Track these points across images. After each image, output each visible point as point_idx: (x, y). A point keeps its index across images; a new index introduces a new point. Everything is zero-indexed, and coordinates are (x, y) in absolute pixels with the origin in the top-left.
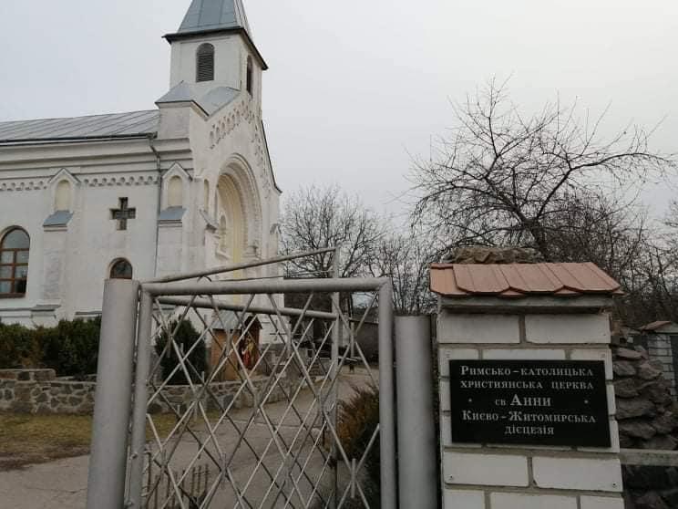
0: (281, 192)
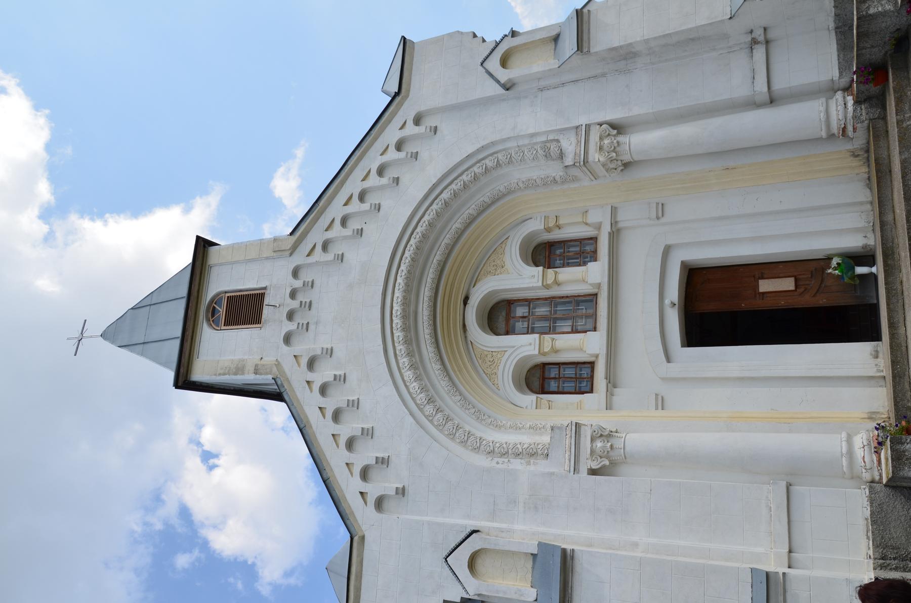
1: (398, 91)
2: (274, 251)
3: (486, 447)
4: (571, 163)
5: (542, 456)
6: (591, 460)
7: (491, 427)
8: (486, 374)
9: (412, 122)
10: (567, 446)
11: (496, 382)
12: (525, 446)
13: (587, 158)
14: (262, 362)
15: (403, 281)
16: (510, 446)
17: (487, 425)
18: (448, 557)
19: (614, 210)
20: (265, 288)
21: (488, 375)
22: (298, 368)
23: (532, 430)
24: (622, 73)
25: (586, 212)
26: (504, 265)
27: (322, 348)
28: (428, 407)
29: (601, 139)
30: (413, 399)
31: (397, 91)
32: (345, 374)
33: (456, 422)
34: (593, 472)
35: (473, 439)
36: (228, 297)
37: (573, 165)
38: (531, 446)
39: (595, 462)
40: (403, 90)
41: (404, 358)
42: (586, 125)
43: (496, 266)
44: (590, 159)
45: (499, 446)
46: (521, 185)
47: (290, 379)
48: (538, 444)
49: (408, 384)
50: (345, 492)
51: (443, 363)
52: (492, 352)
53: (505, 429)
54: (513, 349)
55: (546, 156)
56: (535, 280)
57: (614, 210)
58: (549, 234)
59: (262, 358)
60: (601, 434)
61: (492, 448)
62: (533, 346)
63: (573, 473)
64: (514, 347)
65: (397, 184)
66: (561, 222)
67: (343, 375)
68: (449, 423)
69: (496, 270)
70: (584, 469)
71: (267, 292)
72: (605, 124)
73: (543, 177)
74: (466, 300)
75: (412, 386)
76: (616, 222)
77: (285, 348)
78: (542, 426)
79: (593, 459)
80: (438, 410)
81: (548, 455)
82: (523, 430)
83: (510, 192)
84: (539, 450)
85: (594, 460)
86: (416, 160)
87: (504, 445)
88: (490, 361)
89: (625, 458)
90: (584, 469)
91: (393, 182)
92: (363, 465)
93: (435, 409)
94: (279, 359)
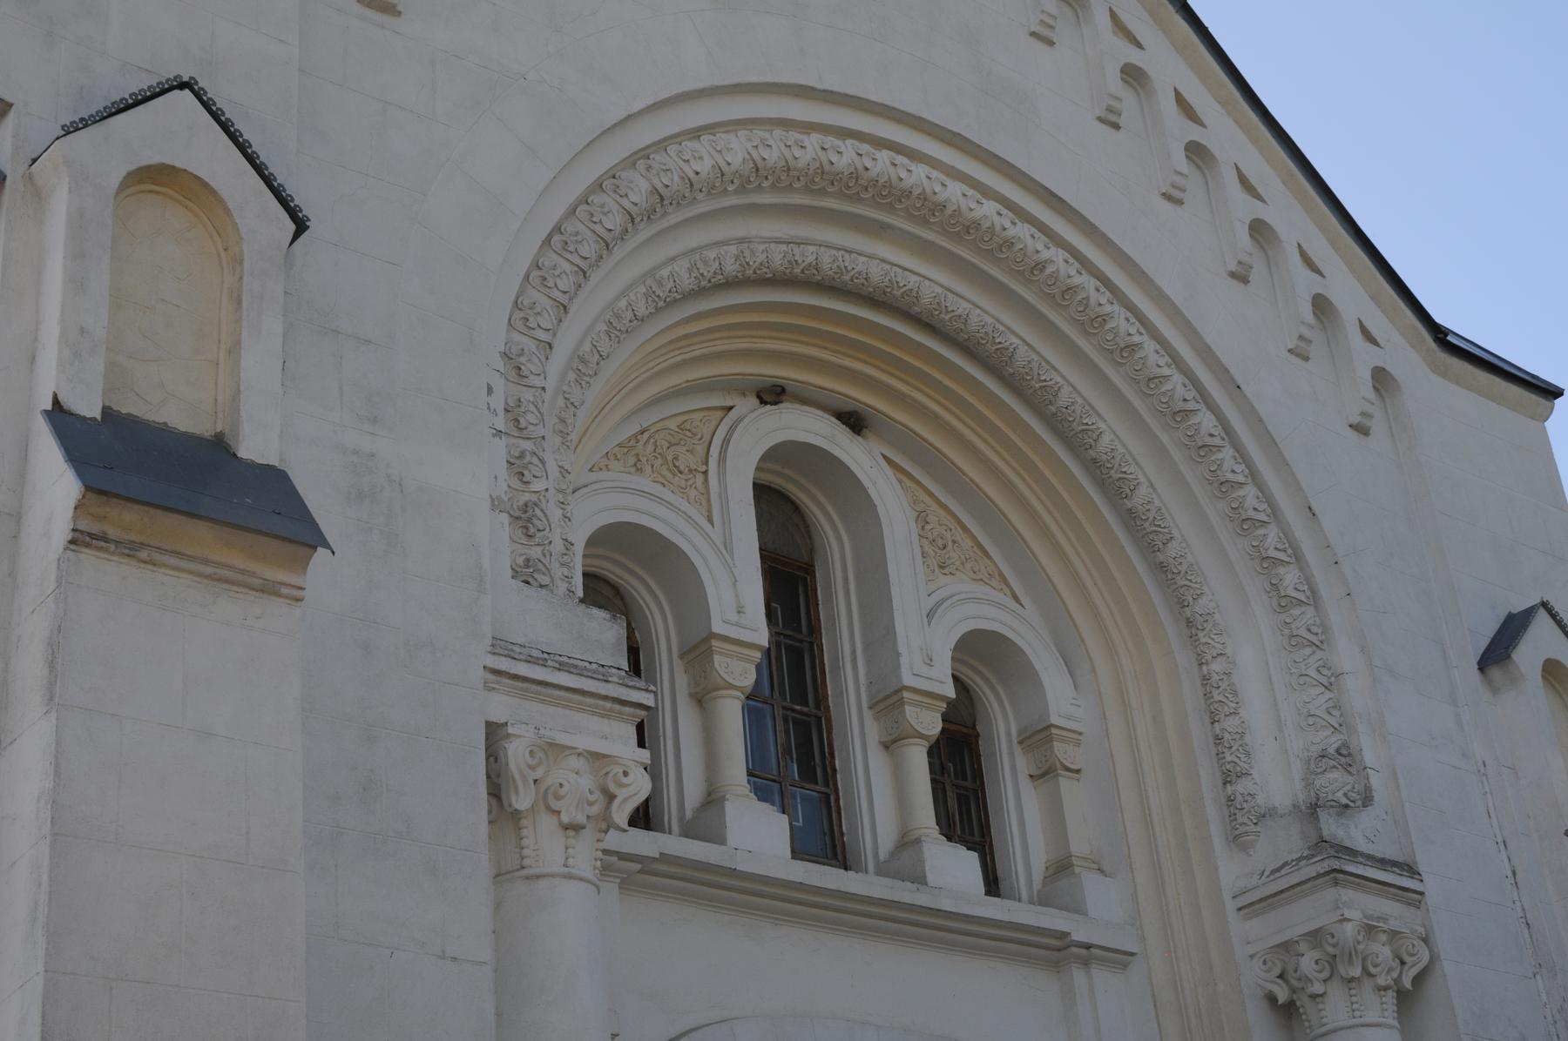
0: (1553, 393)
8: (635, 436)
11: (614, 464)
15: (986, 217)
18: (198, 95)
19: (1119, 959)
24: (1552, 1029)
29: (1394, 934)
34: (495, 733)
42: (1422, 894)
46: (1217, 666)
51: (731, 284)
52: (705, 473)
55: (1323, 756)
57: (1119, 959)
58: (1015, 741)
60: (615, 797)
62: (733, 617)
63: (490, 665)
65: (1233, 275)
66: (1066, 784)
70: (500, 706)
72: (1431, 958)
73: (1248, 739)
74: (854, 421)
76: (1086, 963)
81: (528, 583)
83: (1191, 627)
86: (1290, 351)
88: (676, 458)
89: (528, 878)
90: (500, 706)
91: (1240, 263)
93: (636, 208)
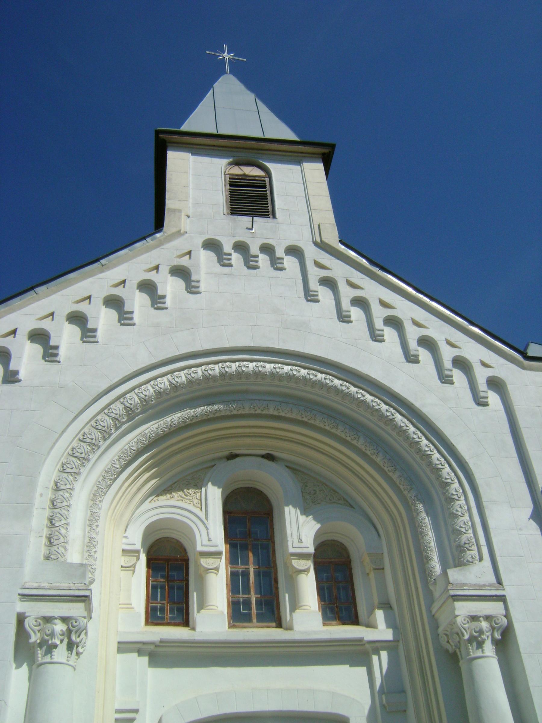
1: (528, 356)
2: (319, 226)
3: (64, 480)
4: (451, 579)
5: (48, 552)
6: (37, 618)
7: (95, 488)
9: (491, 375)
10: (58, 584)
12: (63, 531)
13: (458, 600)
14: (183, 217)
16: (64, 511)
17: (98, 483)
20: (274, 217)
21: (170, 488)
22: (176, 256)
23: (87, 540)
25: (391, 607)
26: (315, 503)
27: (198, 281)
28: (121, 407)
30: (133, 389)
31: (528, 355)
32: (167, 308)
33: (101, 443)
34: (21, 619)
35: (76, 464)
36: (265, 181)
37: (449, 581)
38: (62, 538)
39: (35, 623)
40: (526, 363)
41: (186, 377)
43: (315, 494)
44: (458, 604)
45: (65, 497)
47: (162, 247)
48: (65, 548)
49: (152, 383)
50: (18, 312)
53: (91, 506)
54: (203, 517)
56: (296, 544)
59: (189, 217)
61: (62, 487)
64: (207, 518)
67: (165, 305)
68: (99, 433)
69: (309, 493)
71: (270, 220)
75: (150, 388)
77: (200, 241)
78: (93, 554)
79: (38, 620)
80: (117, 419)
82: (88, 528)
84: (55, 548)
85: (36, 621)
87: (65, 503)
92: (50, 332)
94: (187, 235)
